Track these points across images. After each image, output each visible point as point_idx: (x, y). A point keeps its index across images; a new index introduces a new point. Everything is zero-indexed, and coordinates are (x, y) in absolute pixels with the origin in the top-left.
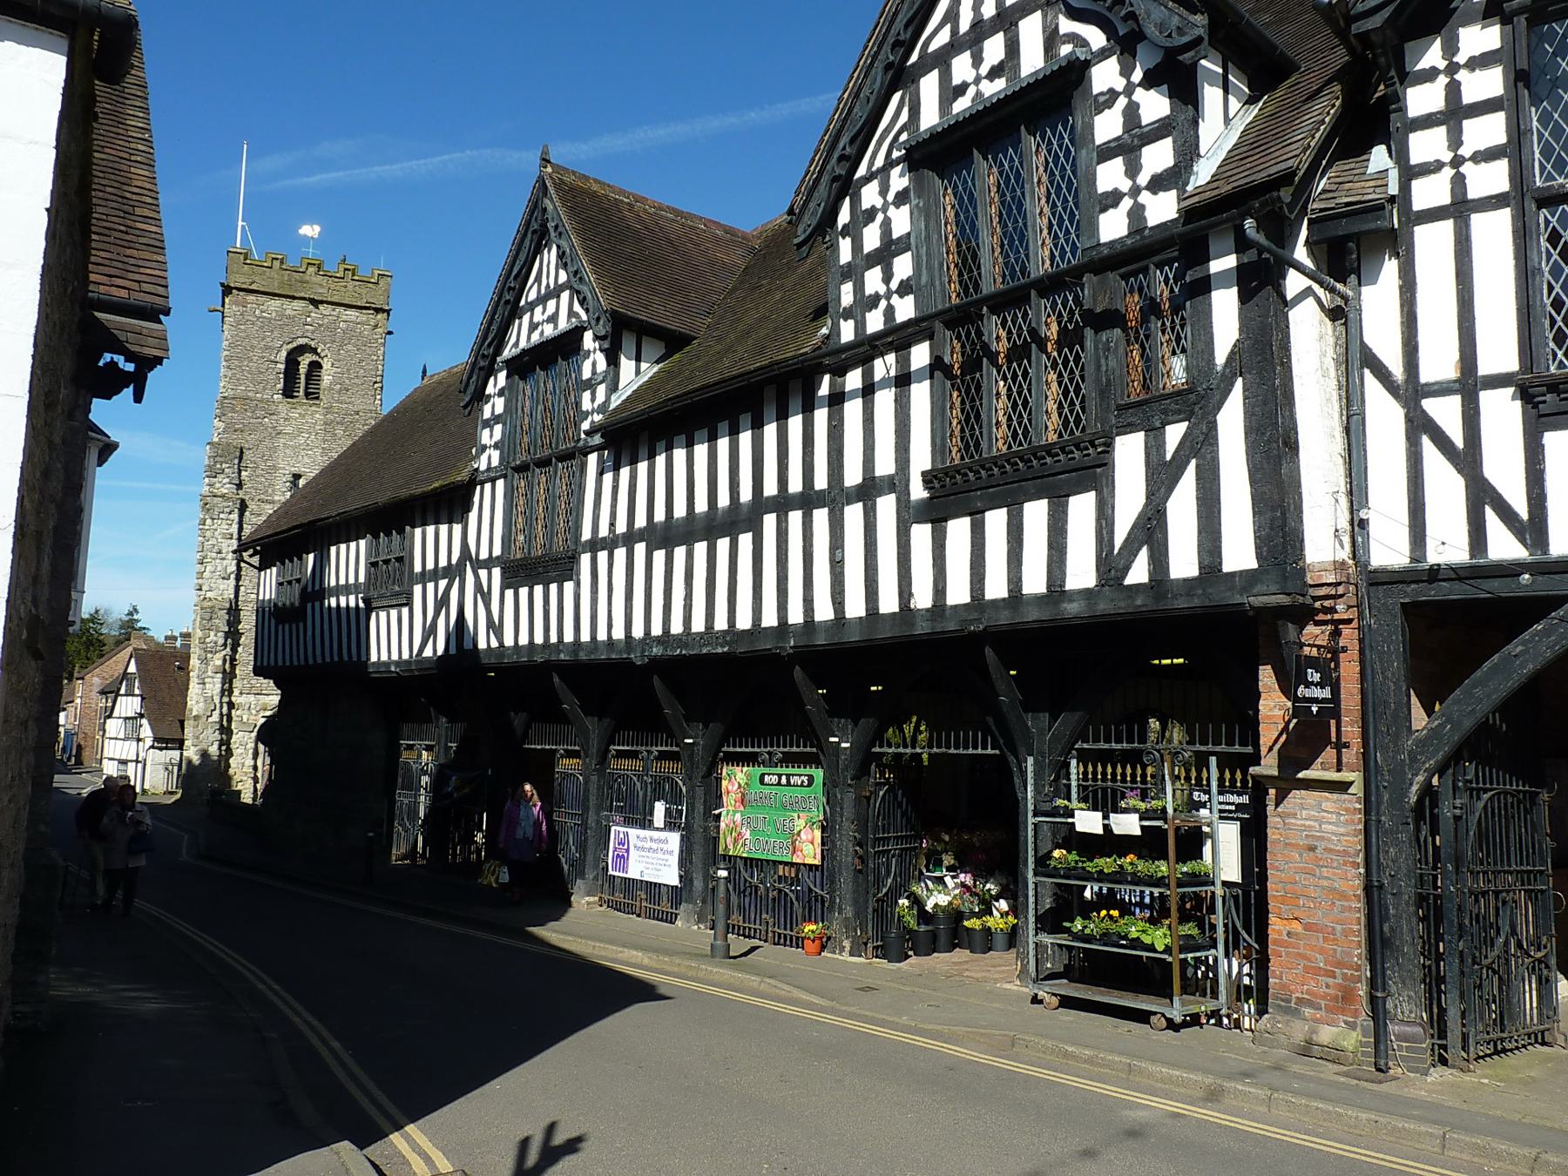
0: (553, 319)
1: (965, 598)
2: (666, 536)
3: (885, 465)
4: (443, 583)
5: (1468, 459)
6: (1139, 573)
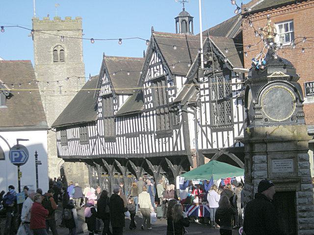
2: (128, 136)
4: (95, 140)
5: (206, 136)
6: (176, 150)
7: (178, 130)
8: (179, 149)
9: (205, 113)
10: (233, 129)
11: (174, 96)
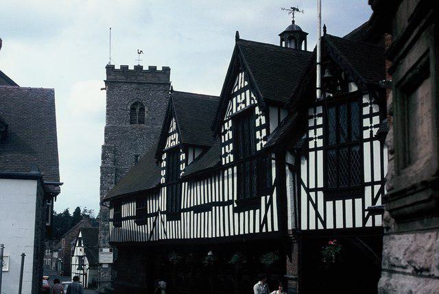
0: (244, 102)
1: (306, 228)
2: (198, 209)
3: (231, 198)
6: (264, 230)
7: (268, 197)
8: (270, 230)
9: (313, 170)
10: (362, 196)
11: (265, 139)
